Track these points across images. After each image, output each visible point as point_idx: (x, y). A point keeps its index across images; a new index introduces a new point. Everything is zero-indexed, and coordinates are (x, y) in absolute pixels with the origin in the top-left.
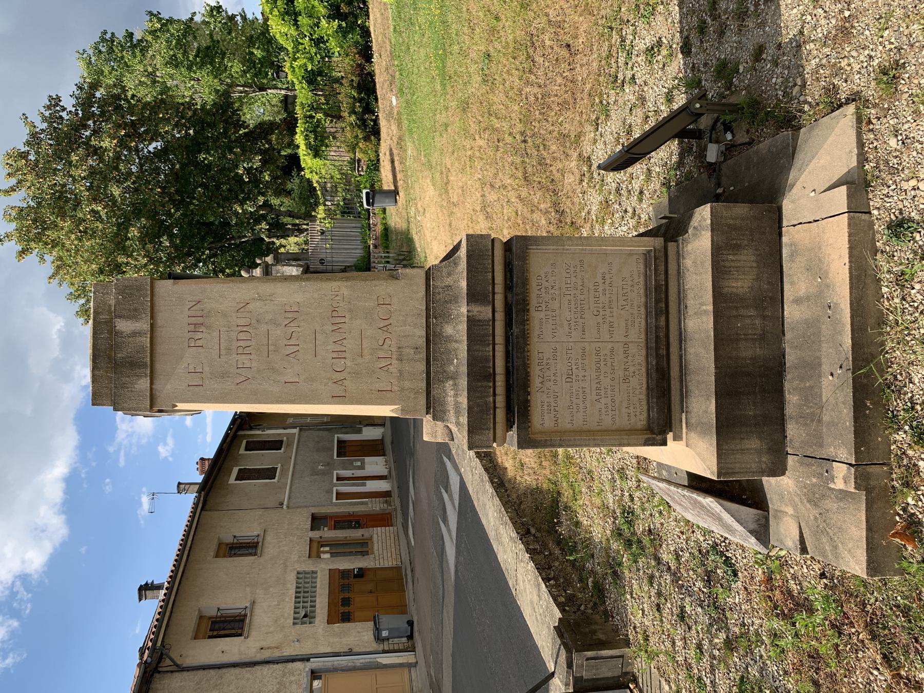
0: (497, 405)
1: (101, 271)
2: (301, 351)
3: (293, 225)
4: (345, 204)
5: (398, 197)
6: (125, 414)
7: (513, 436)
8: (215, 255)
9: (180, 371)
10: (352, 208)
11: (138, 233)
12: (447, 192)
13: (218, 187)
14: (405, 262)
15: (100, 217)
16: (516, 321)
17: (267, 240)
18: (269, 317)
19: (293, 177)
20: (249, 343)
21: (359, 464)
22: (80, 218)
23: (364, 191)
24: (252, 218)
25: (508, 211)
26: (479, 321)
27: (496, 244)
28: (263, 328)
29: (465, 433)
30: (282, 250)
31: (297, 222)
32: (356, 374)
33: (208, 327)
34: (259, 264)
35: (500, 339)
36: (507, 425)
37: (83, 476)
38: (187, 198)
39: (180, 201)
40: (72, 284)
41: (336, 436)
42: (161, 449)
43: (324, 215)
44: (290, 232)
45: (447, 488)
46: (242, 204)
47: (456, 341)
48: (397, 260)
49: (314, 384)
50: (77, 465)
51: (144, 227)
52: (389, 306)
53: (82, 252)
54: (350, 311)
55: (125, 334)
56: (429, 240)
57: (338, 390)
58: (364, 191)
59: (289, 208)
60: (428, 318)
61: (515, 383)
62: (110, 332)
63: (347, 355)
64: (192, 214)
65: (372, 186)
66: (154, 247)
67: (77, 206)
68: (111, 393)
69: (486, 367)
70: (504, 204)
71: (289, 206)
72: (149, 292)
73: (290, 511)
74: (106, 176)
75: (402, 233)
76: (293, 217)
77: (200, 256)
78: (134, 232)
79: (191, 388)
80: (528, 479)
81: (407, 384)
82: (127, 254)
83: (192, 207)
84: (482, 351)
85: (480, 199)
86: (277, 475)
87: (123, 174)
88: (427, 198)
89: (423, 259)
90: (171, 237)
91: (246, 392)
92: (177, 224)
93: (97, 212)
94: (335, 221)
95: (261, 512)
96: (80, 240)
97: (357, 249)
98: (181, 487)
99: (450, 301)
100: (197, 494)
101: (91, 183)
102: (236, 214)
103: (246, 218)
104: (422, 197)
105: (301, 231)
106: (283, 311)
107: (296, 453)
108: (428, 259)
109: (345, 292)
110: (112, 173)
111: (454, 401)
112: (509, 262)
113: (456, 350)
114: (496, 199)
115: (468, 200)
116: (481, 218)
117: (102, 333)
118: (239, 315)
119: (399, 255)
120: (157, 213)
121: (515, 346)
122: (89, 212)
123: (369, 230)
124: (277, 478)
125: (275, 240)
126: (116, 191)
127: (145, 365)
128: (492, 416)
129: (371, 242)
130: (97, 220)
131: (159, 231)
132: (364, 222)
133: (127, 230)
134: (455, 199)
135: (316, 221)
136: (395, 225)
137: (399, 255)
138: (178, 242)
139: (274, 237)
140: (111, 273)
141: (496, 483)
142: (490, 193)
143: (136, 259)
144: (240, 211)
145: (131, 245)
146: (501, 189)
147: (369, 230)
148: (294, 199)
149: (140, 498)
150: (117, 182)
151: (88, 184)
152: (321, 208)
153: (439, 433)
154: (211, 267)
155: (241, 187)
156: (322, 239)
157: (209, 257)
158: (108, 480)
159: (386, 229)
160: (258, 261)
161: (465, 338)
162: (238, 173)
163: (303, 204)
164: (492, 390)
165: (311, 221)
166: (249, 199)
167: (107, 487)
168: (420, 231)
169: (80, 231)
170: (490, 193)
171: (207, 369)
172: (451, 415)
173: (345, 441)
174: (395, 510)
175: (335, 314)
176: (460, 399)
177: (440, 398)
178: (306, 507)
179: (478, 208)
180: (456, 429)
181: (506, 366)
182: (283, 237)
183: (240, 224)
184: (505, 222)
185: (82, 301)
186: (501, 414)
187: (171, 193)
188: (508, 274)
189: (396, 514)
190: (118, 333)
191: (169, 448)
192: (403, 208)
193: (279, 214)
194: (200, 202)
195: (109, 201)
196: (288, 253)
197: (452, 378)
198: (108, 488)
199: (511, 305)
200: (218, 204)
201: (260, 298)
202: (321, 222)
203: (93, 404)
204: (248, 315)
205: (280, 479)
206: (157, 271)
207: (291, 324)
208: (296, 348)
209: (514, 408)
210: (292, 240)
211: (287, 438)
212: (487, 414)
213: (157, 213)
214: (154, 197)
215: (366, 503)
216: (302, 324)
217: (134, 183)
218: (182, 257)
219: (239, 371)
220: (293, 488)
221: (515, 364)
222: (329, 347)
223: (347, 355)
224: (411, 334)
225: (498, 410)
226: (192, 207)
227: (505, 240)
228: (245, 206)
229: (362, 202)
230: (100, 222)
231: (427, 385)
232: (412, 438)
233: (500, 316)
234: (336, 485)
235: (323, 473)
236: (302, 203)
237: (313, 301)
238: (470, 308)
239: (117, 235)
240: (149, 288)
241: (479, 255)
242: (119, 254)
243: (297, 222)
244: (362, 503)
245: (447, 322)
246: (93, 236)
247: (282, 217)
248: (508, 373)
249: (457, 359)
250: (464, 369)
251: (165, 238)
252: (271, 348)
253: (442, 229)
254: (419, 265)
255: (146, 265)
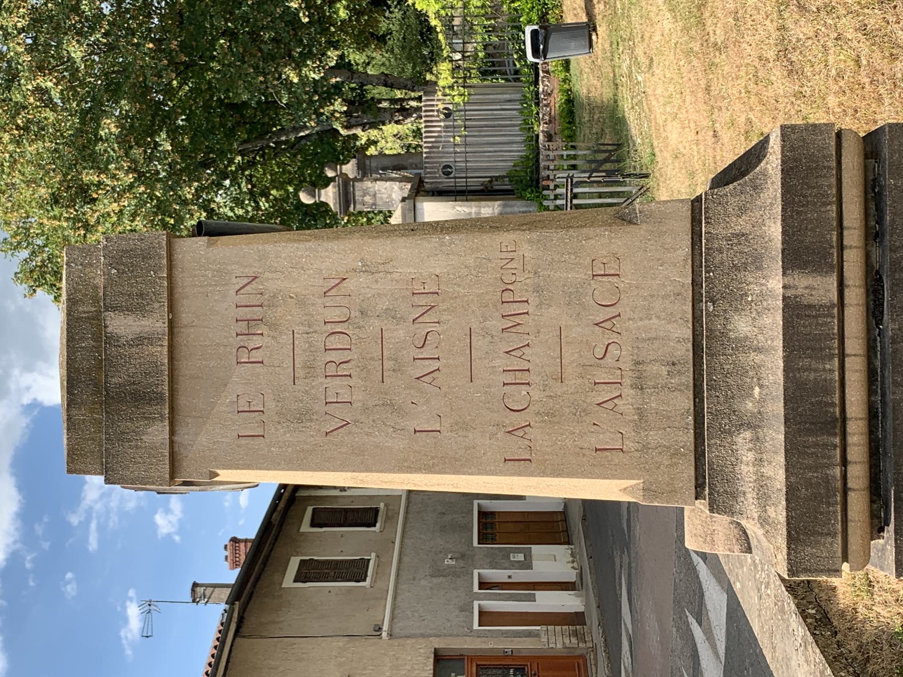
0: (850, 484)
1: (55, 200)
2: (444, 370)
3: (393, 101)
4: (488, 55)
5: (594, 37)
6: (122, 487)
7: (883, 550)
8: (252, 164)
9: (223, 408)
10: (501, 64)
11: (117, 127)
12: (701, 23)
13: (254, 36)
14: (608, 166)
15: (51, 99)
16: (892, 306)
17: (343, 132)
18: (382, 305)
19: (389, 7)
20: (346, 356)
21: (520, 557)
22: (17, 103)
23: (528, 29)
24: (316, 92)
25: (837, 59)
26: (810, 307)
27: (845, 144)
28: (374, 325)
29: (781, 541)
30: (372, 151)
31: (398, 94)
32: (550, 415)
33: (273, 326)
34: (332, 179)
35: (855, 344)
36: (872, 526)
37: (28, 566)
38: (201, 58)
39: (187, 66)
40: (7, 223)
41: (476, 502)
42: (159, 519)
43: (451, 81)
44: (387, 115)
45: (700, 615)
46: (298, 66)
47: (758, 350)
48: (590, 162)
49: (470, 435)
50: (18, 546)
51: (127, 116)
52: (615, 279)
53: (22, 164)
54: (537, 290)
55: (123, 341)
56: (661, 122)
57: (515, 447)
58: (528, 29)
59: (383, 69)
60: (696, 300)
61: (890, 437)
62: (97, 338)
63: (531, 378)
64: (210, 88)
65: (543, 17)
66: (145, 152)
67: (12, 81)
68: (100, 450)
69: (827, 404)
70: (830, 44)
71: (383, 64)
72: (164, 262)
73: (395, 642)
74: (59, 24)
75: (602, 108)
76: (392, 86)
77: (226, 167)
78: (109, 127)
79: (243, 441)
80: (884, 613)
81: (654, 437)
82: (99, 168)
83: (209, 75)
84: (816, 370)
85: (775, 35)
86: (370, 573)
87: (87, 20)
88: (657, 37)
89: (646, 160)
90: (173, 133)
91: (344, 450)
92: (183, 106)
93: (46, 91)
94: (472, 91)
95: (341, 642)
96: (18, 143)
97: (513, 143)
98: (198, 593)
99: (745, 267)
100: (227, 607)
101: (35, 39)
102: (288, 84)
103: (306, 93)
104: (647, 35)
105: (406, 112)
106: (409, 293)
107: (404, 532)
108: (658, 159)
109: (527, 251)
110: (68, 18)
111: (756, 473)
112: (874, 180)
113: (757, 367)
114: (811, 34)
115: (748, 39)
116: (777, 73)
117: (82, 339)
118: (329, 302)
119: (596, 152)
120: (147, 90)
121: (889, 359)
122: (33, 92)
123: (537, 104)
124: (368, 579)
125: (358, 131)
126: (76, 51)
127: (160, 398)
128: (839, 508)
129: (540, 129)
130: (46, 106)
131: (153, 122)
132: (528, 91)
133: (97, 121)
134: (719, 36)
135: (435, 92)
136: (589, 92)
137: (596, 152)
138: (186, 141)
139: (356, 126)
140: (72, 203)
141: (812, 616)
142: (796, 22)
143: (114, 177)
144: (296, 80)
145: (105, 151)
146: (823, 14)
147: (537, 104)
148: (392, 52)
149: (124, 608)
150: (77, 34)
151: (29, 41)
152: (444, 67)
153: (720, 537)
154: (245, 187)
155: (296, 34)
156: (446, 127)
157: (241, 168)
158: (69, 575)
159: (570, 102)
160: (330, 174)
161: (779, 343)
162: (289, 7)
163: (409, 58)
164: (838, 451)
165: (426, 94)
166: (310, 55)
167: (69, 588)
168: (640, 102)
169: (18, 127)
170: (796, 22)
171: (271, 404)
172: (749, 503)
173: (493, 514)
174: (594, 649)
175: (507, 296)
176: (767, 471)
177: (725, 465)
178: (423, 636)
179: (771, 54)
180: (760, 532)
181: (869, 401)
182: (374, 125)
183: (295, 104)
184: (831, 81)
185: (24, 254)
186: (858, 504)
187: (171, 51)
188: (872, 206)
189: (596, 659)
190: (111, 339)
191: (174, 519)
192: (604, 59)
193: (365, 80)
194: (224, 65)
195: (66, 70)
196: (382, 155)
197: (749, 426)
198: (71, 590)
199: (877, 272)
200: (256, 68)
201: (367, 269)
202: (445, 95)
203: (70, 471)
204: (345, 302)
205: (374, 581)
206: (151, 197)
207: (425, 318)
208: (435, 365)
209: (888, 491)
210: (390, 129)
211: (386, 505)
212: (829, 504)
213: (147, 90)
214: (143, 59)
215: (537, 635)
216: (444, 318)
217: (106, 35)
218: (195, 170)
219: (330, 408)
220: (399, 599)
221: (890, 397)
222: (497, 362)
223: (531, 378)
224: (661, 334)
225: (852, 495)
226: (209, 75)
227: (862, 134)
228: (304, 70)
229: (524, 51)
230: (51, 110)
231: (696, 438)
232: (625, 513)
233: (855, 296)
234: (478, 597)
235: (453, 573)
236: (408, 58)
237: (464, 271)
238: (789, 280)
239: (80, 132)
240: (164, 253)
241: (809, 168)
242: (85, 168)
243: (398, 94)
244: (529, 634)
245: (737, 310)
246: (39, 137)
247: (370, 87)
248: (873, 415)
249: (761, 386)
250: (777, 408)
251: (164, 135)
252: (388, 364)
253: (688, 99)
254: (638, 171)
255: (131, 186)
